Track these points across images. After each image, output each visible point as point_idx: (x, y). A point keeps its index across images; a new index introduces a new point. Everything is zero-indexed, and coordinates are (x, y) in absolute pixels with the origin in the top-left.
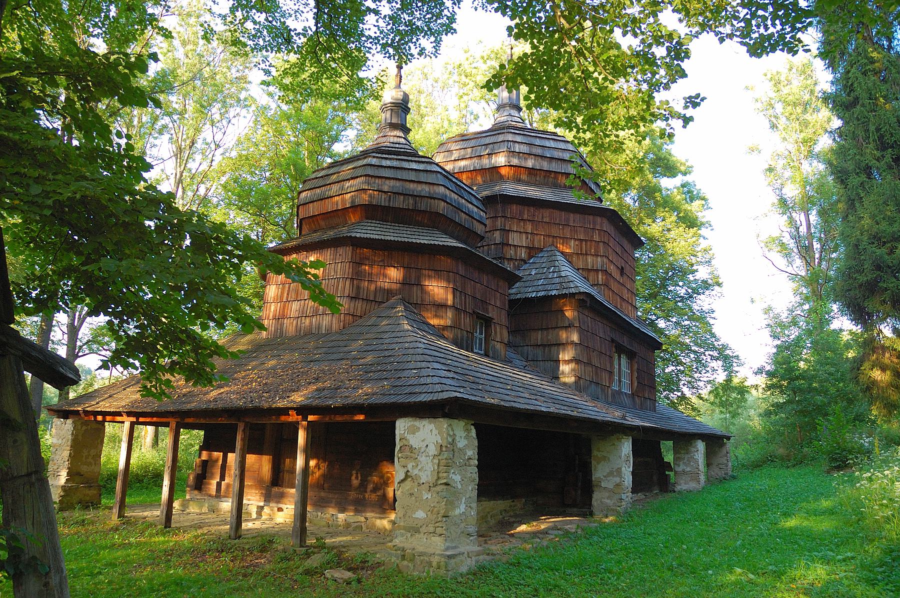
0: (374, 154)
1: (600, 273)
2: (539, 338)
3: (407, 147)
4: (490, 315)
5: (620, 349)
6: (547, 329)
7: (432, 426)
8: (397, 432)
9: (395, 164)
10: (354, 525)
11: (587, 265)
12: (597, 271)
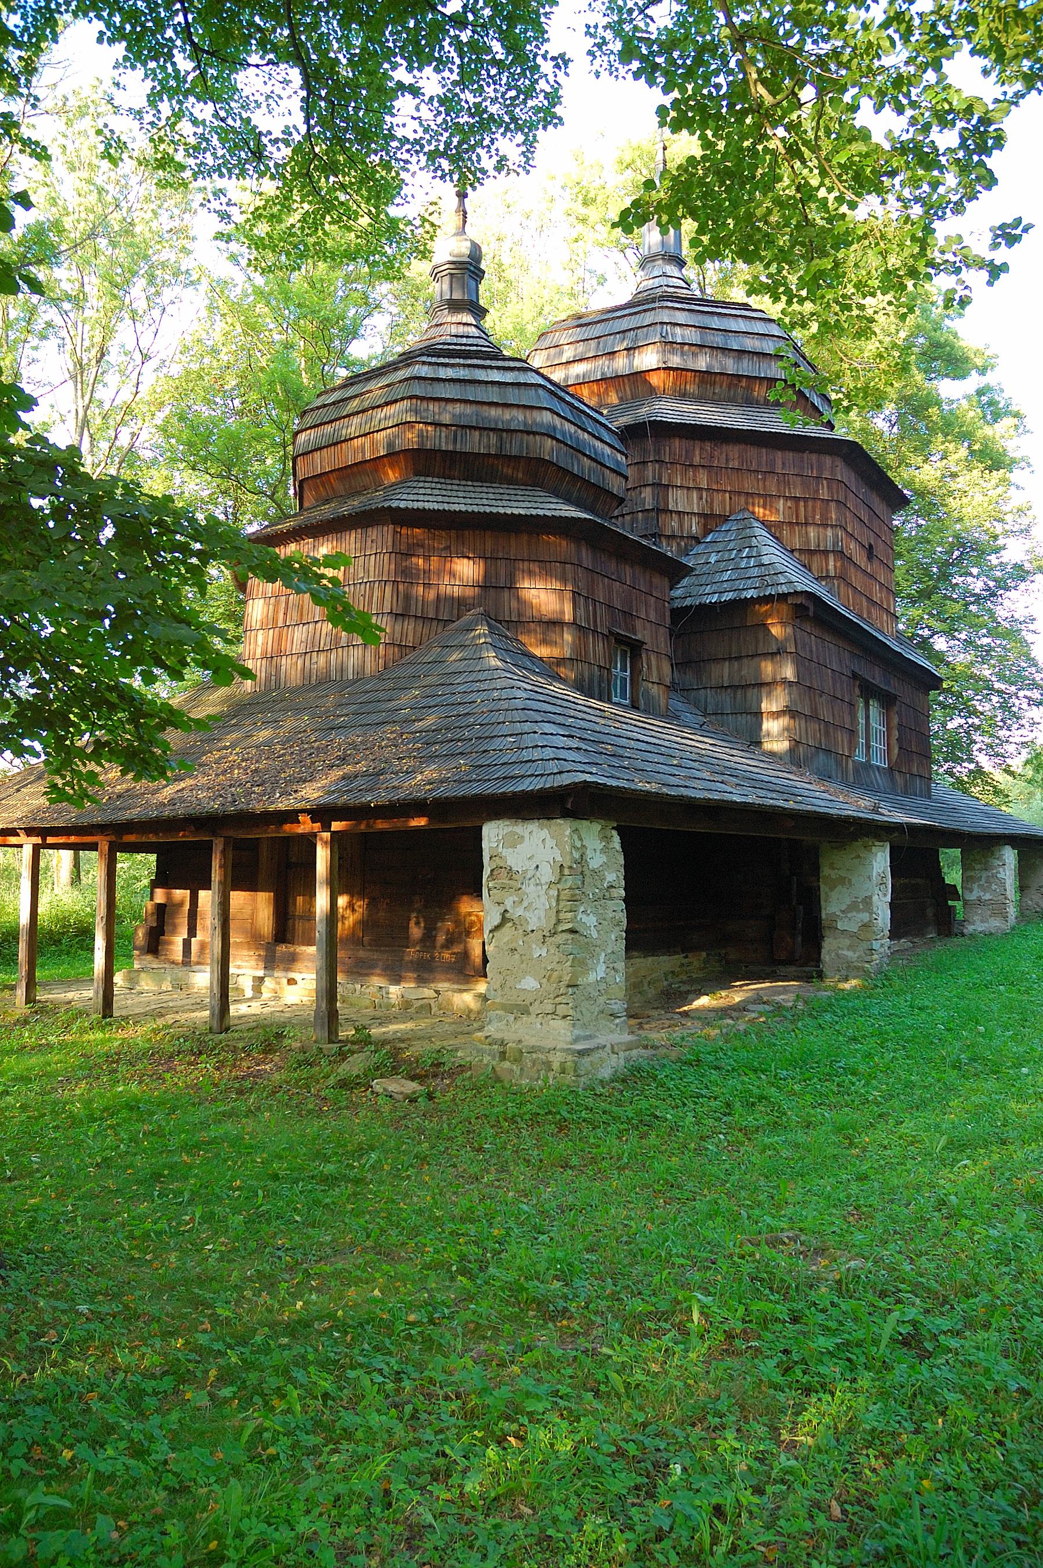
0: (424, 359)
4: (639, 637)
5: (868, 691)
7: (544, 833)
8: (485, 845)
9: (462, 373)
12: (825, 553)
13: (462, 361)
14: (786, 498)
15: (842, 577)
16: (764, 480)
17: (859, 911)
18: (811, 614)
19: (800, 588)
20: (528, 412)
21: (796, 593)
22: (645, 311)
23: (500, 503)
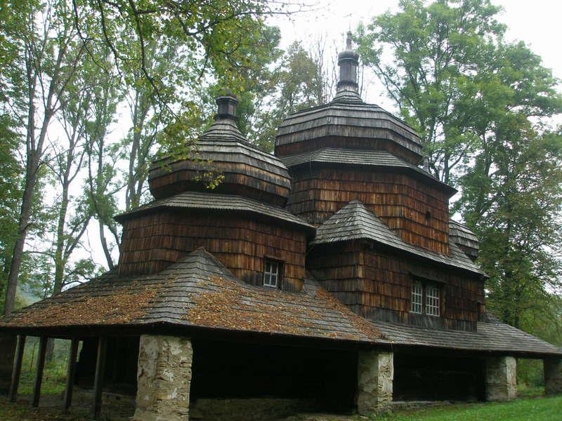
2: (336, 274)
6: (342, 267)
8: (140, 343)
9: (210, 149)
12: (395, 218)
14: (377, 194)
15: (404, 229)
20: (234, 165)
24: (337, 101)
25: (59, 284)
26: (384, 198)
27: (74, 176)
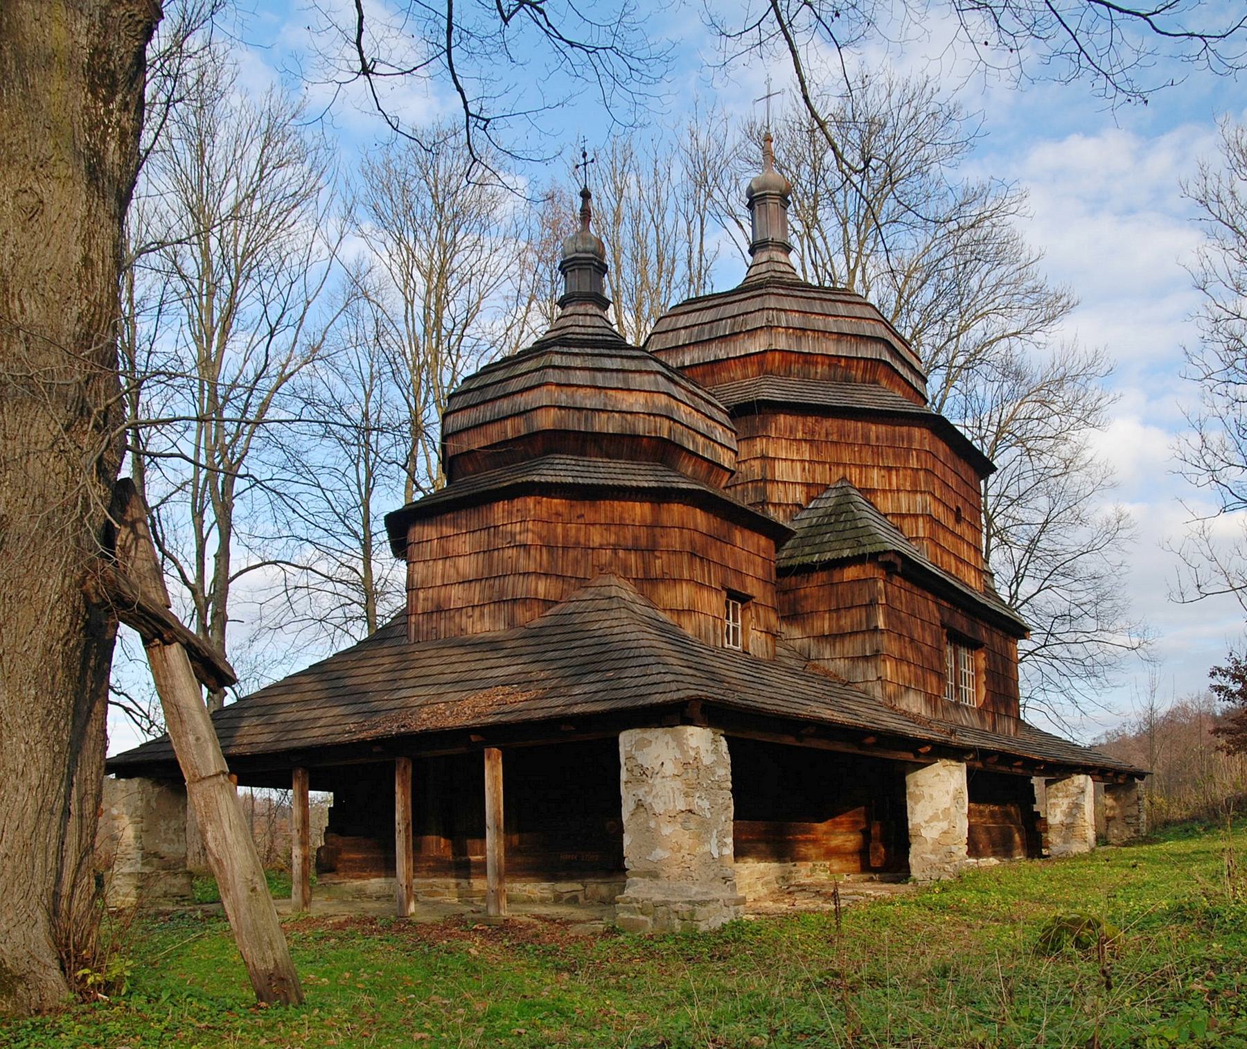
0: (557, 349)
1: (921, 519)
3: (606, 331)
4: (749, 592)
5: (957, 639)
7: (668, 738)
8: (621, 749)
9: (589, 363)
10: (568, 896)
11: (900, 507)
12: (916, 516)
13: (589, 351)
16: (860, 452)
17: (939, 820)
18: (899, 570)
19: (890, 547)
21: (886, 552)
22: (753, 297)
23: (626, 477)
24: (748, 289)
25: (517, 346)
26: (894, 477)
27: (361, 18)
